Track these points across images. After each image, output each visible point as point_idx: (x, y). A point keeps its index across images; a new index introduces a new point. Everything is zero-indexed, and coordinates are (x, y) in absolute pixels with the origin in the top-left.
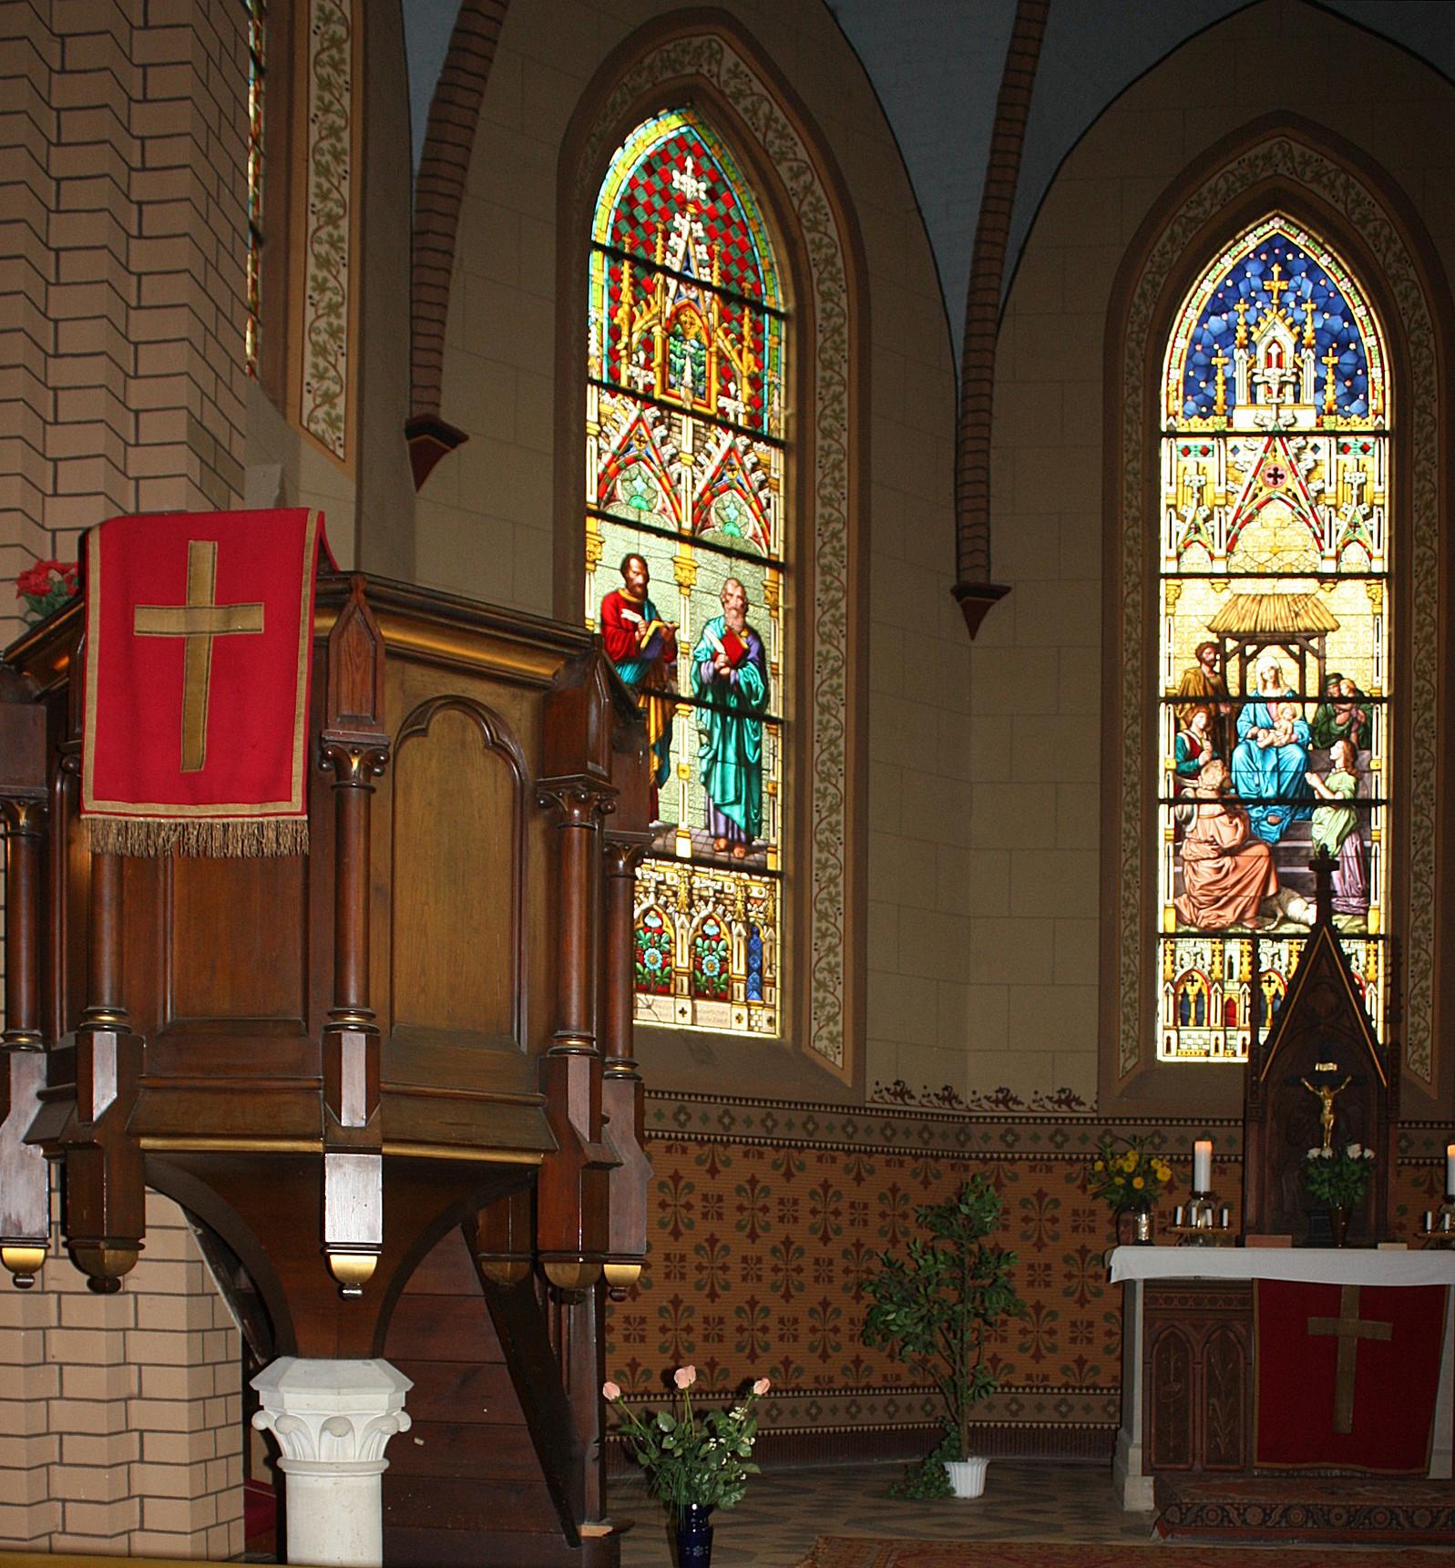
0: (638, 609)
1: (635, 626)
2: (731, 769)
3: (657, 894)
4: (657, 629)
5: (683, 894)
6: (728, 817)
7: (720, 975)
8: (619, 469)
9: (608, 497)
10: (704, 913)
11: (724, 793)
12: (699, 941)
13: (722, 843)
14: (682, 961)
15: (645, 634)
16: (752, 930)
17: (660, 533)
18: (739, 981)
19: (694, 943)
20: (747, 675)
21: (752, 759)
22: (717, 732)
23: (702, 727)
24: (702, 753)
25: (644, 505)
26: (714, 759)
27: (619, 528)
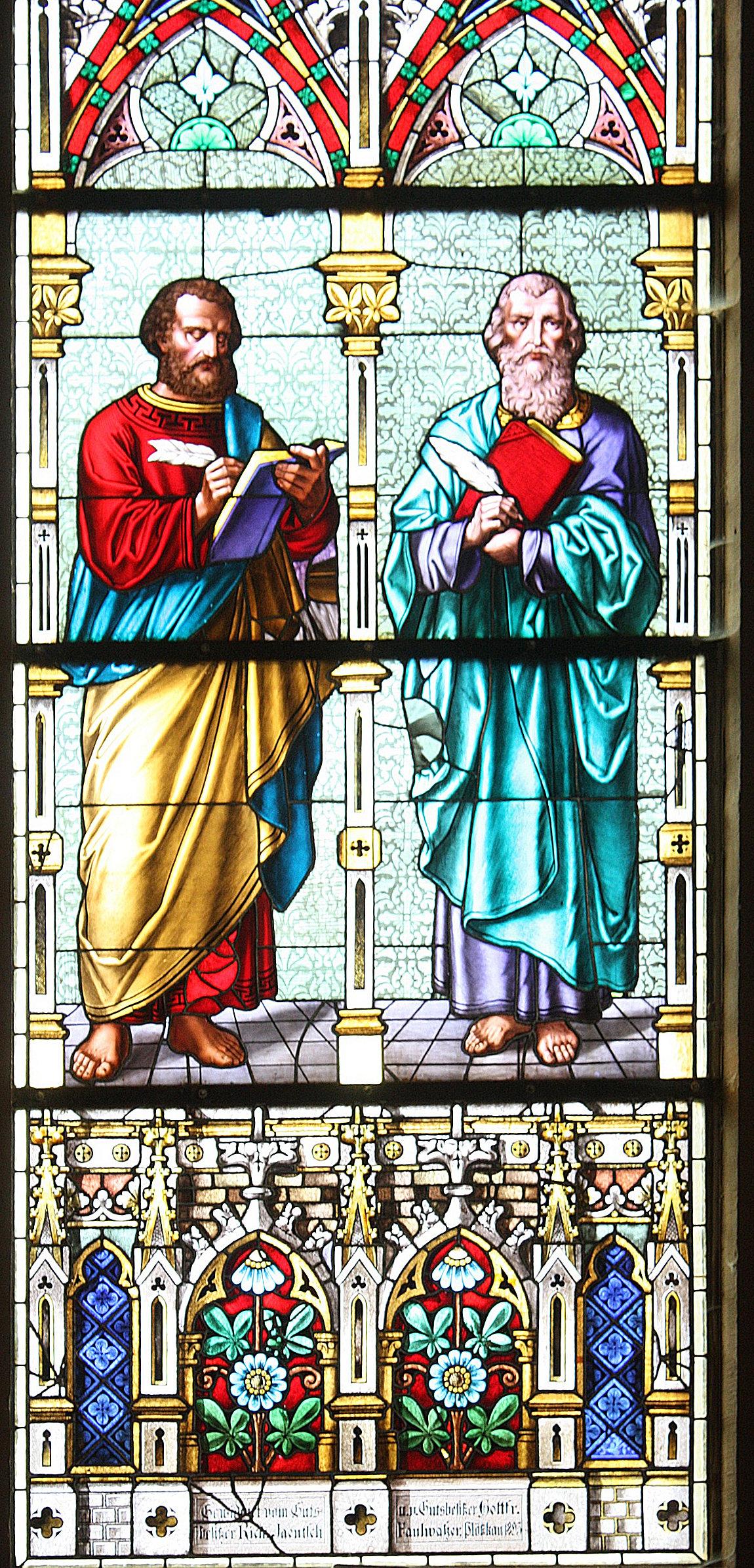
0: (206, 430)
1: (194, 477)
2: (524, 819)
3: (270, 1204)
4: (268, 471)
5: (359, 1195)
6: (514, 952)
7: (487, 1402)
8: (136, 57)
9: (93, 125)
10: (431, 1233)
11: (498, 886)
12: (416, 1315)
13: (495, 1029)
14: (357, 1377)
15: (223, 484)
16: (602, 1260)
17: (272, 201)
18: (557, 1410)
19: (199, 1326)
20: (588, 536)
21: (599, 765)
22: (472, 719)
23: (419, 711)
24: (423, 785)
25: (217, 136)
26: (468, 795)
27: (140, 224)
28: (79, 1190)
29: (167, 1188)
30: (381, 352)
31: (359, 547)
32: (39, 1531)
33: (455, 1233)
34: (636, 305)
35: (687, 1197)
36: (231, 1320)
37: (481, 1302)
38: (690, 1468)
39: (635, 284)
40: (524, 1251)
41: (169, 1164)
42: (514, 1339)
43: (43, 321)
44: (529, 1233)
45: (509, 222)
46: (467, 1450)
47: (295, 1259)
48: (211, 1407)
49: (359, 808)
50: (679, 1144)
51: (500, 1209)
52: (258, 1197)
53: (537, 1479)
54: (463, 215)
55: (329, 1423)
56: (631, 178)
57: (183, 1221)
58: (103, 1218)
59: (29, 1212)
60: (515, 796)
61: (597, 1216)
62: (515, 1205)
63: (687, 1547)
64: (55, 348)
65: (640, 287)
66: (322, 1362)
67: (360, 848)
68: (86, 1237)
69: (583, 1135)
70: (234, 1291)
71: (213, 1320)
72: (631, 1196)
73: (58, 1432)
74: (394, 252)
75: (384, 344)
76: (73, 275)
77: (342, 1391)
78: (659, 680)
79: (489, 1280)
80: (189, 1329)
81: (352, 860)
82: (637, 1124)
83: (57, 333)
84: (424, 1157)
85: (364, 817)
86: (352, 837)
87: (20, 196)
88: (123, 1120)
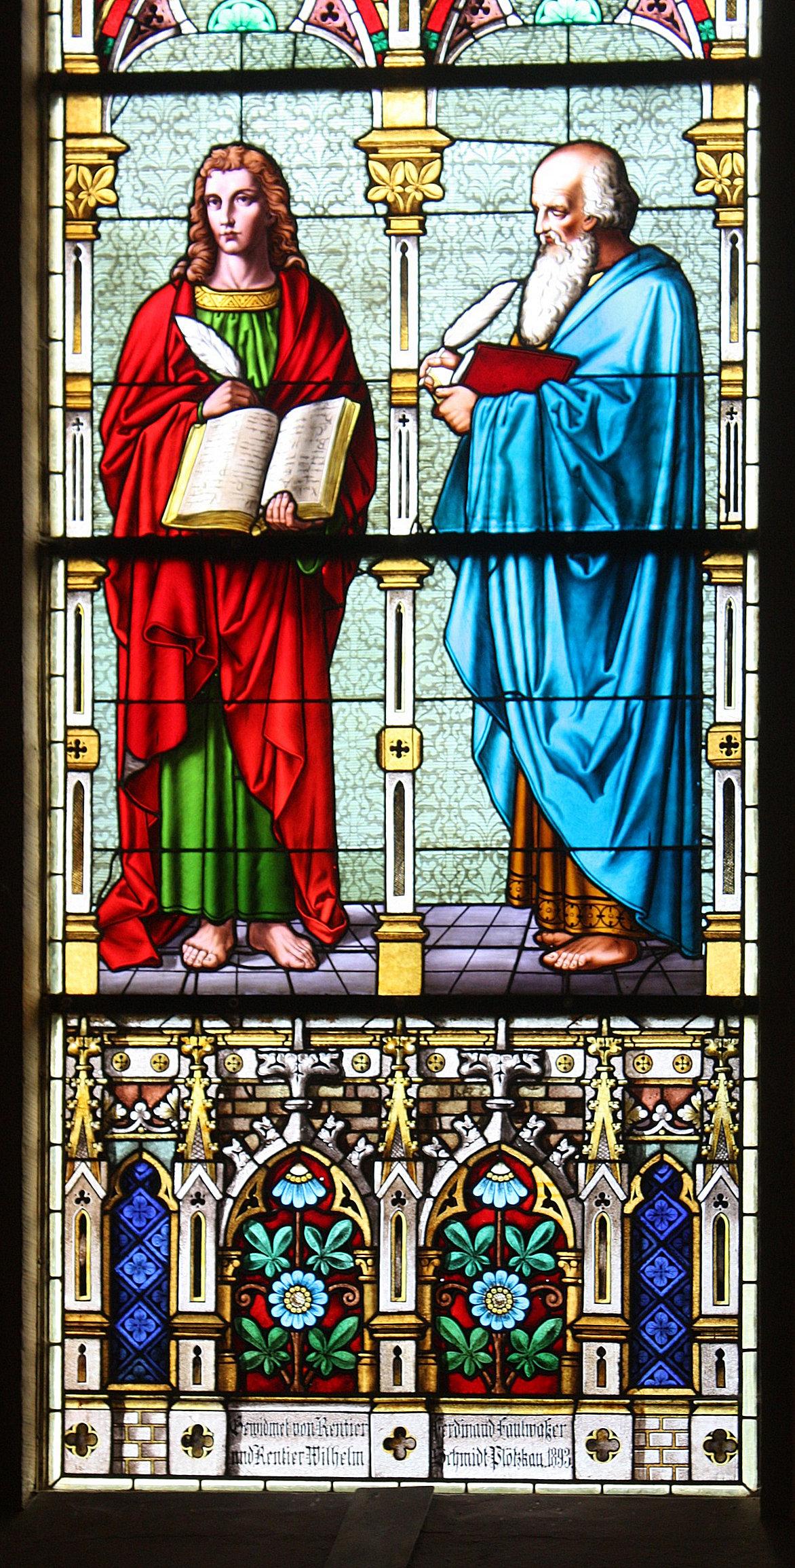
7: (529, 1325)
28: (639, 1102)
29: (408, 1097)
30: (425, 233)
31: (400, 433)
32: (74, 1448)
33: (295, 1149)
34: (688, 179)
35: (738, 1116)
36: (271, 1235)
37: (523, 1220)
38: (738, 1399)
39: (686, 158)
40: (367, 1164)
41: (409, 1073)
42: (557, 1259)
43: (77, 201)
44: (370, 1149)
45: (152, 103)
46: (307, 1372)
47: (538, 1172)
48: (451, 1327)
49: (729, 704)
50: (613, 1061)
51: (340, 1125)
52: (299, 1109)
53: (698, 1406)
54: (182, 97)
55: (570, 1345)
56: (676, 49)
57: (222, 1135)
58: (662, 1132)
59: (64, 1124)
60: (561, 695)
61: (119, 1133)
62: (555, 1120)
63: (68, 1471)
64: (89, 229)
65: (692, 161)
66: (362, 1278)
67: (399, 749)
68: (121, 1149)
69: (223, 1048)
70: (474, 1203)
71: (253, 1237)
72: (157, 1111)
73: (93, 1348)
74: (436, 128)
75: (101, 229)
76: (434, 149)
77: (381, 1310)
78: (380, 580)
79: (531, 1198)
80: (429, 1245)
81: (391, 761)
82: (569, 1039)
83: (91, 215)
84: (264, 1071)
85: (405, 717)
86: (391, 737)
87: (101, 68)
88: (683, 1029)
